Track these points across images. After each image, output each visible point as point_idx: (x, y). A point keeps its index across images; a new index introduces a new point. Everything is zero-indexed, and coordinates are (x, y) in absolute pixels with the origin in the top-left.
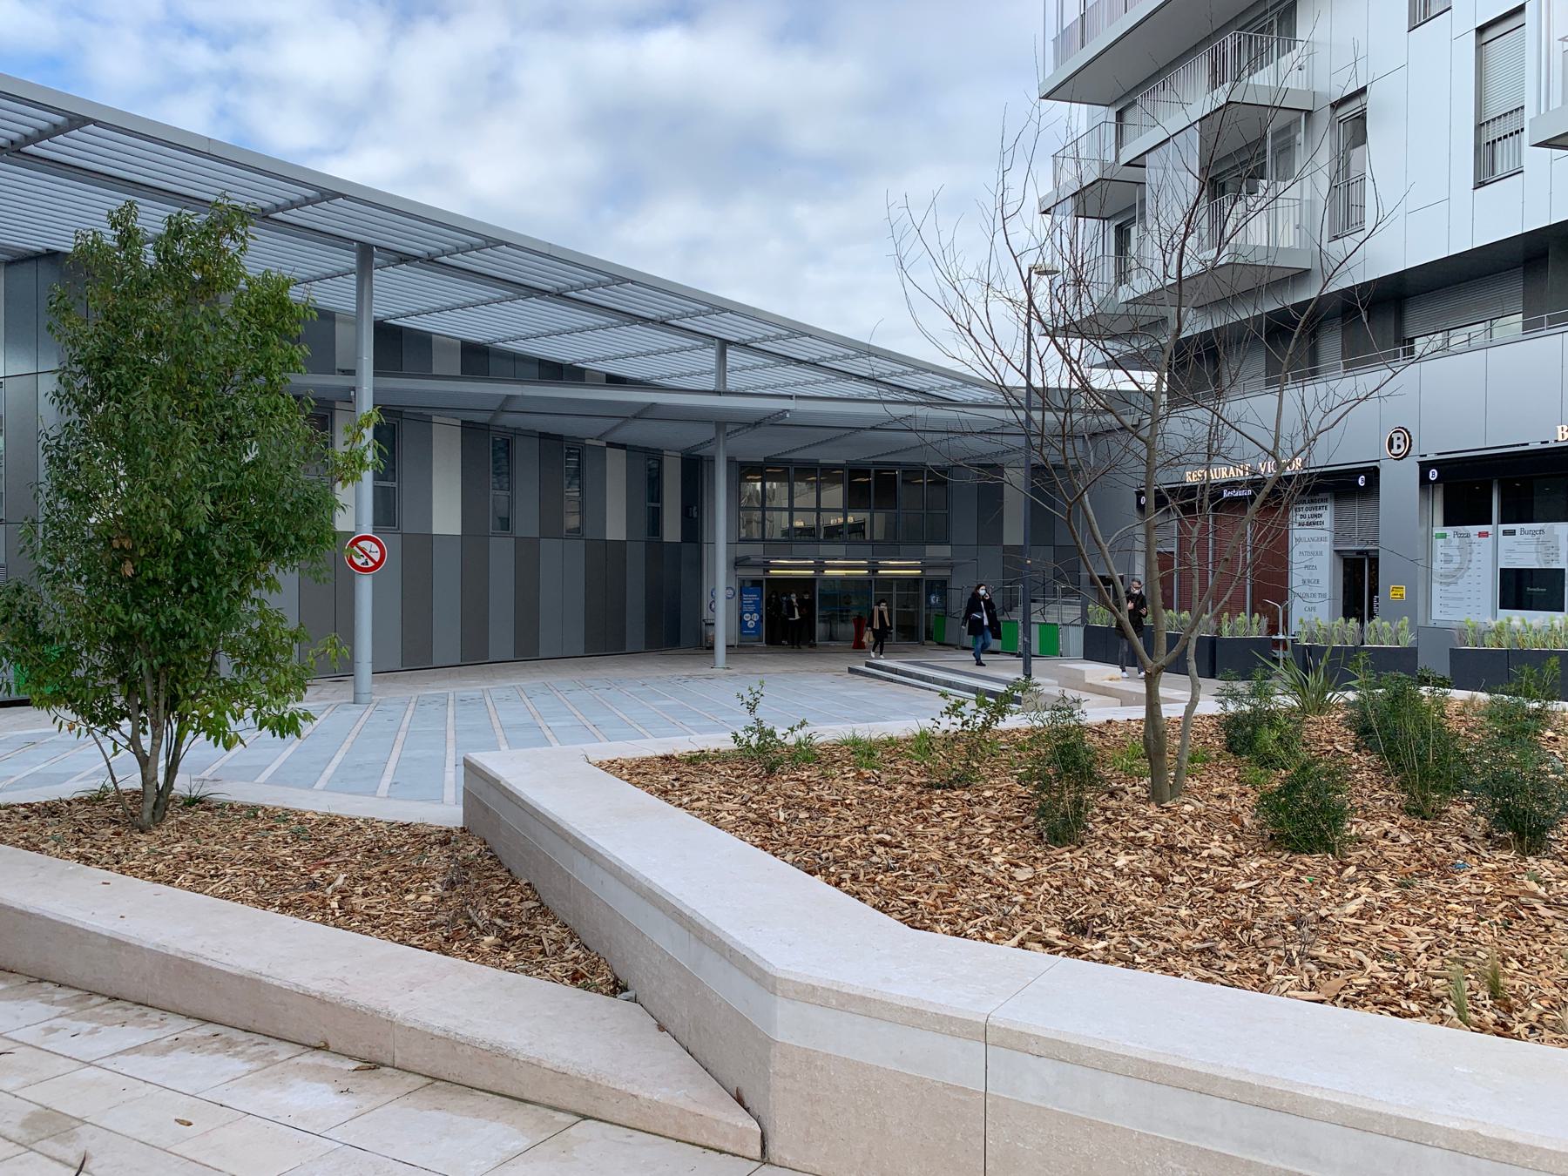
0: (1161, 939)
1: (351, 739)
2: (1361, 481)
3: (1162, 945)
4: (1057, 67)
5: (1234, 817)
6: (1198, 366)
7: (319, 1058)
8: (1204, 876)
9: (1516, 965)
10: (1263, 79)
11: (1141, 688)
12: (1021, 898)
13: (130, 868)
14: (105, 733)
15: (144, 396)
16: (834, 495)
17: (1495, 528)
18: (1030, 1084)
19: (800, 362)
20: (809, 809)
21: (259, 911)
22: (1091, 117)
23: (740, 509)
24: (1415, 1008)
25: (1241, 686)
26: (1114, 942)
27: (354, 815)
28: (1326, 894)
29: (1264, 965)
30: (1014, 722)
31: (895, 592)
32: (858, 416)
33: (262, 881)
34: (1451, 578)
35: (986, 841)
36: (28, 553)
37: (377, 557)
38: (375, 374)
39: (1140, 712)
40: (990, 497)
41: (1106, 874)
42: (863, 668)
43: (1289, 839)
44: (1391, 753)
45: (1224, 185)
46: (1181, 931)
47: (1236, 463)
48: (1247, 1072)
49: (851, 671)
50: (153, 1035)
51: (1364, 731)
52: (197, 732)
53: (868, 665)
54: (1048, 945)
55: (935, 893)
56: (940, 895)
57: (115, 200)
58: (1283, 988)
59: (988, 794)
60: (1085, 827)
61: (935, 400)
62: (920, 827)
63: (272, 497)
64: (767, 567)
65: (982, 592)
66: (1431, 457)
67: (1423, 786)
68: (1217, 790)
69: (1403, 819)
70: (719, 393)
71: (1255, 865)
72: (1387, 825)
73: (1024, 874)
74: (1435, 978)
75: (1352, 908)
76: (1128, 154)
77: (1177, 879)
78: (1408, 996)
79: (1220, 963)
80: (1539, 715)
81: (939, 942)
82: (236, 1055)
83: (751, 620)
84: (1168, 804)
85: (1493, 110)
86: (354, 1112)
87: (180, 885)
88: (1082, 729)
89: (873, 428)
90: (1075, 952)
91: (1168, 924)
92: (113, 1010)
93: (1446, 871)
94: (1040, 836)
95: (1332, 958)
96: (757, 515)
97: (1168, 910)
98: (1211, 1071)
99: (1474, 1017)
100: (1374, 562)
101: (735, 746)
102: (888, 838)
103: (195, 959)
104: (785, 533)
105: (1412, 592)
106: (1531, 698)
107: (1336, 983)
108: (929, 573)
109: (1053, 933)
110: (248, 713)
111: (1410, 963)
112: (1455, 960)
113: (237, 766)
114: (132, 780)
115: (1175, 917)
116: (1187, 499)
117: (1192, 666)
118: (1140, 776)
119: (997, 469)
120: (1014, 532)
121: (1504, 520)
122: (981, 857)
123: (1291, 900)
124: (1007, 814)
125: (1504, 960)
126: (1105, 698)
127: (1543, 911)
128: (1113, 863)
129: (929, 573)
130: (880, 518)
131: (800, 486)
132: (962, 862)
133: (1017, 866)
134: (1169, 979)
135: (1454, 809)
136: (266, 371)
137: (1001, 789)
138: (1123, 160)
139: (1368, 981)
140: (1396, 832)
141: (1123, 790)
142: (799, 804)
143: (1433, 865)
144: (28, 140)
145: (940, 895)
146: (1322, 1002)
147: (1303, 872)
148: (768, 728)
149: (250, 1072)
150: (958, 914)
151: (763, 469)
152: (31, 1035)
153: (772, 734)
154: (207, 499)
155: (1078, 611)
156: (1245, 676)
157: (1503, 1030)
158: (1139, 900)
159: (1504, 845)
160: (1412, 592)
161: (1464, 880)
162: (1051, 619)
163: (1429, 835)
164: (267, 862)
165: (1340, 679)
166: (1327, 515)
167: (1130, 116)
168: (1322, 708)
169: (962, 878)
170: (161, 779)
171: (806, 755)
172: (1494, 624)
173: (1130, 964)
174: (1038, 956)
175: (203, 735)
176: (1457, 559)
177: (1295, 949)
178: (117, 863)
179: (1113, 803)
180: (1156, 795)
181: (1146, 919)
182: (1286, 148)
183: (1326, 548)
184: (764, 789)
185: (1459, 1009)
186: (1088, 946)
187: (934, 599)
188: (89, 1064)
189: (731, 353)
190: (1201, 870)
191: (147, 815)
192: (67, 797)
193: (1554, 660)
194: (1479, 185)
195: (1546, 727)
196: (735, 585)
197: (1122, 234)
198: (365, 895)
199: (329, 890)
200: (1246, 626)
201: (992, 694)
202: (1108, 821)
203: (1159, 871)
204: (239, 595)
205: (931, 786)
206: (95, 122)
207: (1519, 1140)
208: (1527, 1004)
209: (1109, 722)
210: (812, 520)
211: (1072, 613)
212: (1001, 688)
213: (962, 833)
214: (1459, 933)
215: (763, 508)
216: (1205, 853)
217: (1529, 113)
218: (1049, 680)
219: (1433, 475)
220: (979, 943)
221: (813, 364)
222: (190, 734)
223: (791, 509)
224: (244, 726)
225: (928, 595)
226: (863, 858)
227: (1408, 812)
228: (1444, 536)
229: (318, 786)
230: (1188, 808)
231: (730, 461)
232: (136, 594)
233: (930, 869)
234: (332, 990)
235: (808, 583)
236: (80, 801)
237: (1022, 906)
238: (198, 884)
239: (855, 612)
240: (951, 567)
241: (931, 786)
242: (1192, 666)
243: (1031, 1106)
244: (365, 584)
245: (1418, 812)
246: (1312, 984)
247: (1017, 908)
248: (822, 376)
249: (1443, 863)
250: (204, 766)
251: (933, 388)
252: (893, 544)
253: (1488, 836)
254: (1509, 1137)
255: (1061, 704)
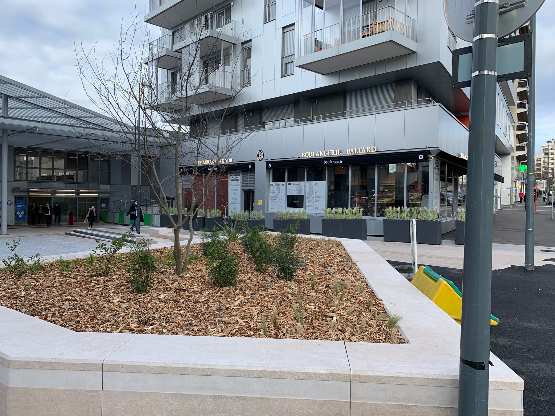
0: (173, 322)
2: (250, 167)
3: (173, 324)
4: (150, 11)
5: (202, 277)
6: (199, 124)
8: (191, 298)
9: (282, 315)
10: (221, 30)
11: (173, 235)
12: (123, 314)
16: (60, 163)
17: (286, 183)
18: (119, 383)
19: (44, 108)
20: (36, 290)
22: (163, 32)
23: (15, 167)
24: (252, 333)
25: (210, 234)
26: (156, 326)
28: (229, 300)
29: (207, 326)
30: (125, 250)
31: (87, 203)
32: (59, 130)
34: (274, 198)
35: (112, 294)
39: (173, 244)
40: (126, 168)
41: (156, 302)
42: (72, 233)
43: (218, 283)
44: (252, 252)
45: (208, 64)
46: (181, 318)
47: (205, 158)
48: (197, 364)
49: (67, 234)
51: (246, 246)
53: (74, 231)
54: (131, 330)
55: (88, 316)
56: (90, 317)
58: (212, 333)
59: (114, 277)
60: (150, 286)
61: (104, 129)
62: (85, 292)
64: (28, 192)
65: (136, 203)
66: (269, 160)
67: (261, 262)
68: (198, 268)
69: (255, 273)
70: (4, 117)
71: (208, 293)
72: (250, 275)
73: (124, 306)
74: (259, 323)
75: (237, 303)
76: (177, 47)
77: (181, 300)
78: (250, 330)
79: (192, 328)
80: (294, 239)
81: (88, 336)
83: (21, 214)
84: (181, 275)
85: (287, 54)
88: (149, 252)
89: (77, 137)
90: (141, 331)
91: (176, 317)
93: (265, 288)
94: (133, 290)
95: (231, 321)
96: (24, 170)
97: (176, 312)
98: (186, 366)
99: (268, 333)
100: (253, 193)
101: (4, 266)
102: (70, 298)
104: (38, 178)
105: (264, 202)
106: (292, 233)
107: (229, 329)
108: (101, 195)
109: (133, 326)
111: (252, 319)
112: (265, 316)
115: (179, 314)
116: (190, 170)
117: (191, 226)
118: (173, 266)
119: (128, 157)
120: (134, 181)
121: (288, 181)
122: (109, 301)
123: (218, 303)
124: (122, 284)
125: (279, 314)
126: (159, 239)
127: (290, 297)
128: (159, 297)
129: (101, 195)
130: (81, 173)
131: (44, 159)
132: (101, 303)
133: (123, 302)
134: (175, 336)
135: (270, 268)
137: (120, 275)
138: (174, 50)
139: (239, 327)
140: (252, 277)
141: (166, 271)
142: (32, 288)
143: (262, 287)
145: (90, 317)
146: (224, 336)
147: (223, 293)
148: (20, 257)
150: (97, 324)
151: (27, 151)
153: (22, 260)
155: (158, 209)
156: (210, 231)
157: (276, 336)
158: (167, 310)
159: (281, 278)
160: (264, 202)
161: (270, 290)
162: (149, 212)
163: (262, 277)
165: (239, 230)
166: (240, 177)
167: (176, 34)
168: (235, 239)
169: (100, 309)
171: (38, 268)
172: (285, 212)
173: (161, 333)
174: (127, 335)
176: (276, 192)
177: (217, 319)
179: (162, 276)
180: (177, 272)
181: (169, 316)
182: (227, 55)
183: (239, 188)
184: (15, 283)
185: (264, 332)
186: (146, 329)
187: (103, 205)
189: (10, 102)
190: (190, 296)
193: (298, 221)
194: (283, 76)
195: (296, 242)
196: (13, 200)
197: (174, 76)
200: (215, 213)
201: (118, 239)
202: (159, 283)
203: (175, 299)
205: (92, 276)
207: (278, 370)
208: (284, 327)
209: (165, 248)
210: (50, 173)
211: (156, 210)
212: (120, 237)
213: (102, 293)
214: (267, 307)
215: (27, 168)
216: (192, 290)
217: (296, 56)
218: (145, 234)
219: (270, 166)
220: (104, 333)
221: (50, 110)
223: (40, 168)
225: (101, 203)
226: (58, 307)
227: (256, 270)
228: (272, 185)
230: (188, 275)
231: (10, 147)
233: (87, 308)
235: (48, 199)
237: (123, 317)
239: (69, 211)
240: (110, 193)
241: (92, 276)
242: (191, 226)
243: (120, 392)
245: (259, 270)
246: (222, 330)
247: (121, 318)
248: (54, 115)
249: (265, 286)
251: (81, 117)
252: (86, 184)
253: (278, 276)
254: (275, 370)
255: (142, 241)
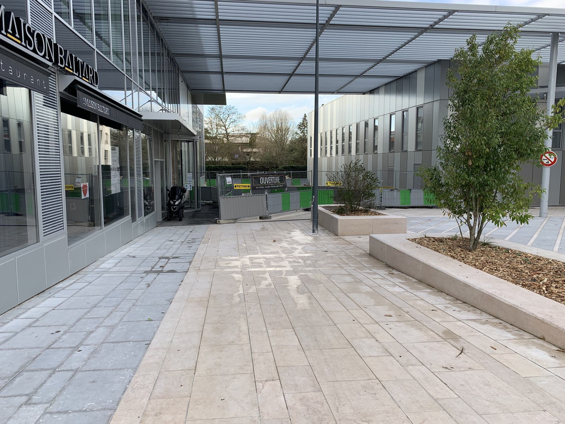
1: (539, 230)
7: (541, 342)
13: (468, 262)
14: (458, 218)
15: (478, 102)
21: (514, 284)
27: (547, 257)
33: (514, 275)
36: (439, 158)
37: (553, 160)
38: (556, 86)
50: (479, 317)
52: (489, 220)
57: (468, 37)
63: (522, 135)
82: (509, 332)
86: (558, 365)
87: (484, 271)
92: (464, 306)
103: (493, 296)
110: (508, 215)
113: (502, 233)
114: (467, 234)
136: (521, 89)
144: (436, 23)
149: (515, 339)
152: (441, 307)
154: (498, 136)
164: (515, 269)
170: (476, 235)
175: (491, 221)
178: (462, 260)
188: (460, 321)
191: (471, 246)
192: (445, 237)
198: (556, 287)
199: (541, 283)
204: (507, 172)
206: (457, 11)
222: (486, 221)
224: (506, 219)
229: (529, 244)
232: (471, 171)
234: (547, 319)
236: (449, 239)
238: (491, 271)
244: (547, 172)
250: (491, 232)
